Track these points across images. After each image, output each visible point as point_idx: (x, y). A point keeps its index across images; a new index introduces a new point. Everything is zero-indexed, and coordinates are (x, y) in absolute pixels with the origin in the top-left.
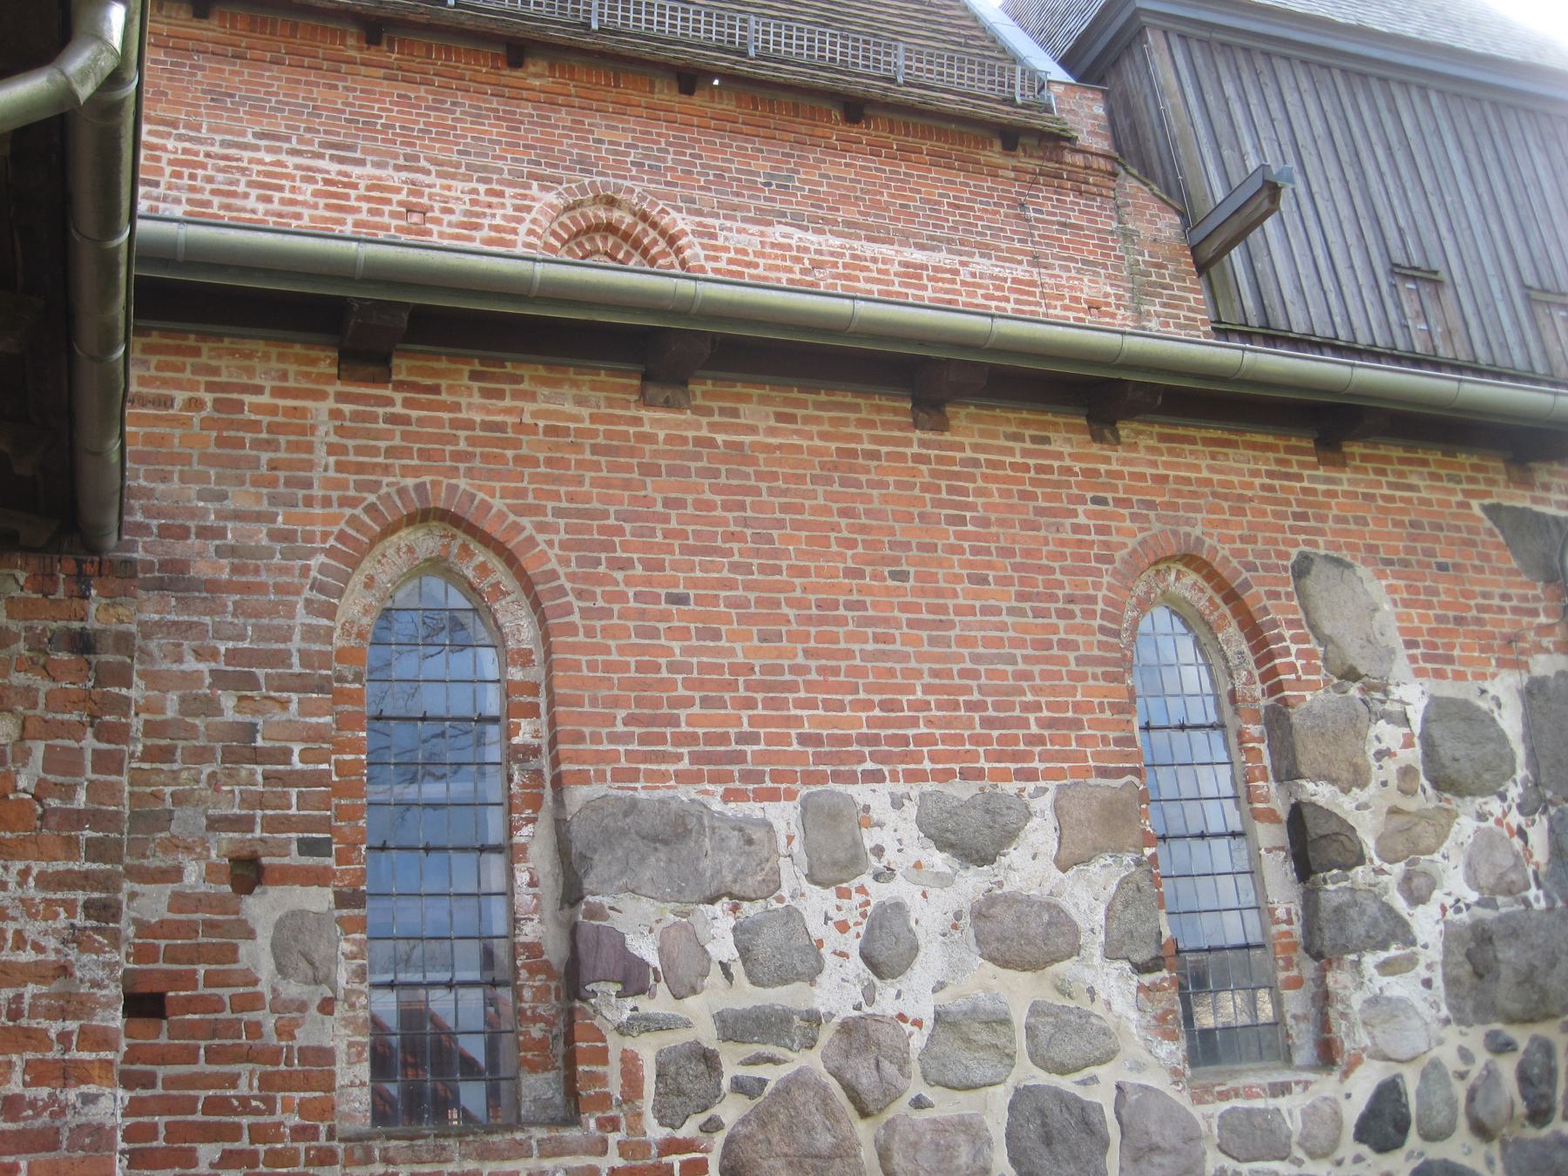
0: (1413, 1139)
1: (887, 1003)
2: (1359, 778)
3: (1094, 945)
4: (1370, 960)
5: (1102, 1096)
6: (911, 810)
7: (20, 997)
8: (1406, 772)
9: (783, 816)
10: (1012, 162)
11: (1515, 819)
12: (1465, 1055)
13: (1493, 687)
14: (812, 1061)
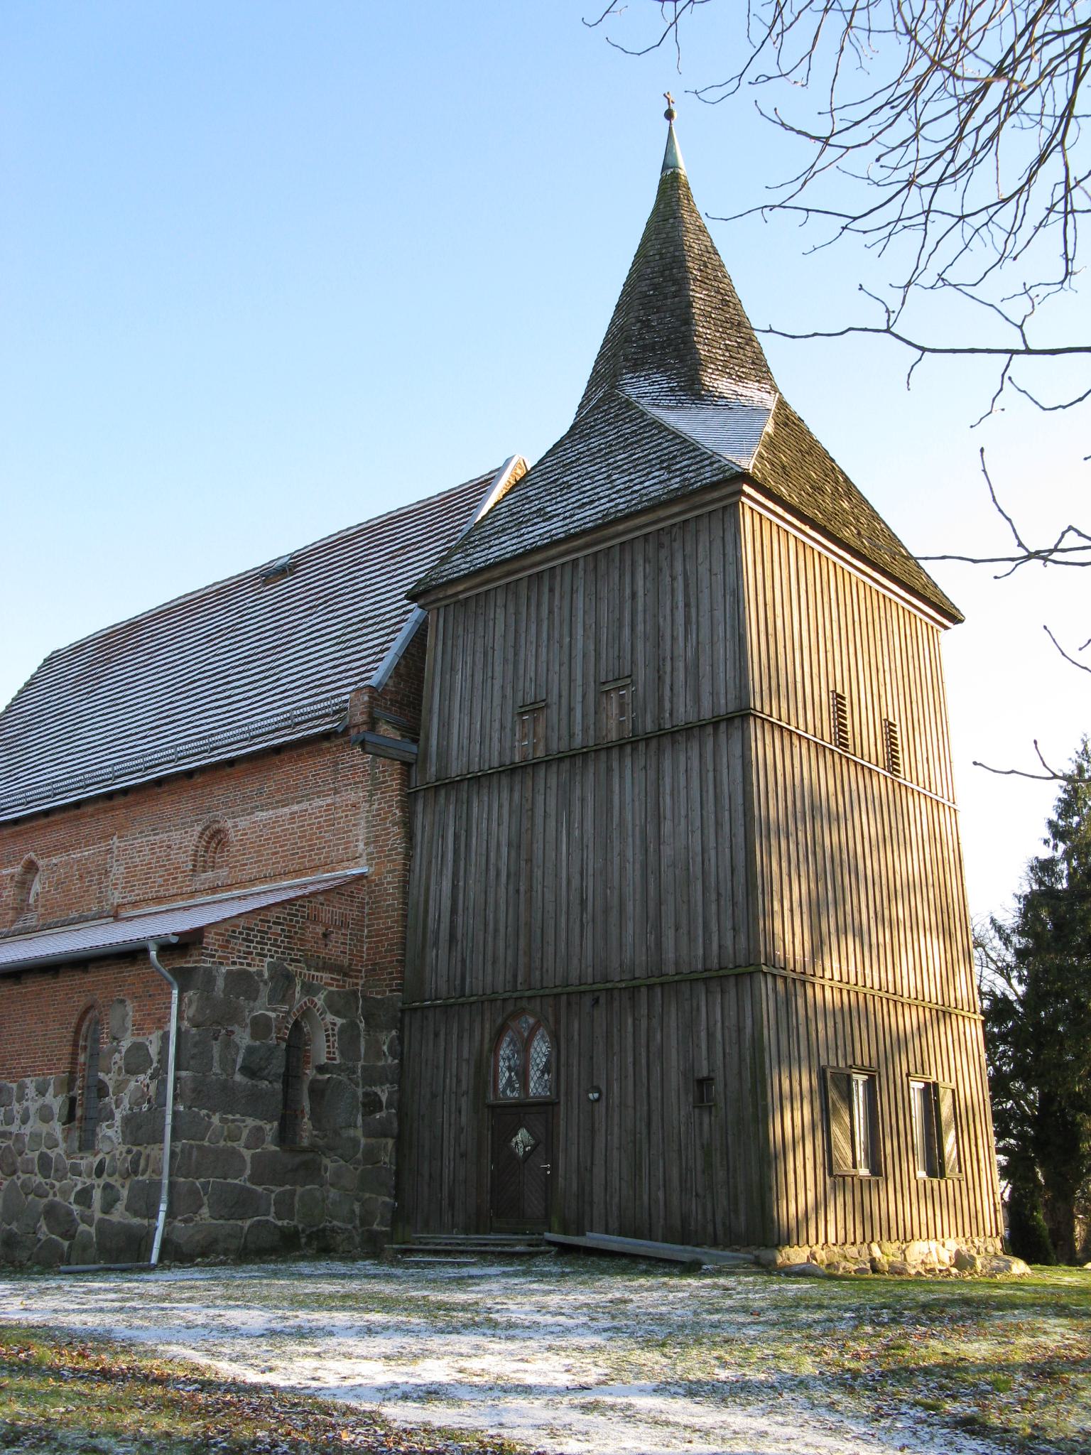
0: (105, 1175)
1: (22, 1131)
2: (108, 1072)
3: (56, 1117)
5: (53, 1155)
6: (34, 1084)
7: (293, 1193)
8: (120, 1068)
9: (14, 1085)
10: (333, 745)
11: (148, 1081)
12: (121, 1154)
13: (151, 1037)
14: (11, 1143)
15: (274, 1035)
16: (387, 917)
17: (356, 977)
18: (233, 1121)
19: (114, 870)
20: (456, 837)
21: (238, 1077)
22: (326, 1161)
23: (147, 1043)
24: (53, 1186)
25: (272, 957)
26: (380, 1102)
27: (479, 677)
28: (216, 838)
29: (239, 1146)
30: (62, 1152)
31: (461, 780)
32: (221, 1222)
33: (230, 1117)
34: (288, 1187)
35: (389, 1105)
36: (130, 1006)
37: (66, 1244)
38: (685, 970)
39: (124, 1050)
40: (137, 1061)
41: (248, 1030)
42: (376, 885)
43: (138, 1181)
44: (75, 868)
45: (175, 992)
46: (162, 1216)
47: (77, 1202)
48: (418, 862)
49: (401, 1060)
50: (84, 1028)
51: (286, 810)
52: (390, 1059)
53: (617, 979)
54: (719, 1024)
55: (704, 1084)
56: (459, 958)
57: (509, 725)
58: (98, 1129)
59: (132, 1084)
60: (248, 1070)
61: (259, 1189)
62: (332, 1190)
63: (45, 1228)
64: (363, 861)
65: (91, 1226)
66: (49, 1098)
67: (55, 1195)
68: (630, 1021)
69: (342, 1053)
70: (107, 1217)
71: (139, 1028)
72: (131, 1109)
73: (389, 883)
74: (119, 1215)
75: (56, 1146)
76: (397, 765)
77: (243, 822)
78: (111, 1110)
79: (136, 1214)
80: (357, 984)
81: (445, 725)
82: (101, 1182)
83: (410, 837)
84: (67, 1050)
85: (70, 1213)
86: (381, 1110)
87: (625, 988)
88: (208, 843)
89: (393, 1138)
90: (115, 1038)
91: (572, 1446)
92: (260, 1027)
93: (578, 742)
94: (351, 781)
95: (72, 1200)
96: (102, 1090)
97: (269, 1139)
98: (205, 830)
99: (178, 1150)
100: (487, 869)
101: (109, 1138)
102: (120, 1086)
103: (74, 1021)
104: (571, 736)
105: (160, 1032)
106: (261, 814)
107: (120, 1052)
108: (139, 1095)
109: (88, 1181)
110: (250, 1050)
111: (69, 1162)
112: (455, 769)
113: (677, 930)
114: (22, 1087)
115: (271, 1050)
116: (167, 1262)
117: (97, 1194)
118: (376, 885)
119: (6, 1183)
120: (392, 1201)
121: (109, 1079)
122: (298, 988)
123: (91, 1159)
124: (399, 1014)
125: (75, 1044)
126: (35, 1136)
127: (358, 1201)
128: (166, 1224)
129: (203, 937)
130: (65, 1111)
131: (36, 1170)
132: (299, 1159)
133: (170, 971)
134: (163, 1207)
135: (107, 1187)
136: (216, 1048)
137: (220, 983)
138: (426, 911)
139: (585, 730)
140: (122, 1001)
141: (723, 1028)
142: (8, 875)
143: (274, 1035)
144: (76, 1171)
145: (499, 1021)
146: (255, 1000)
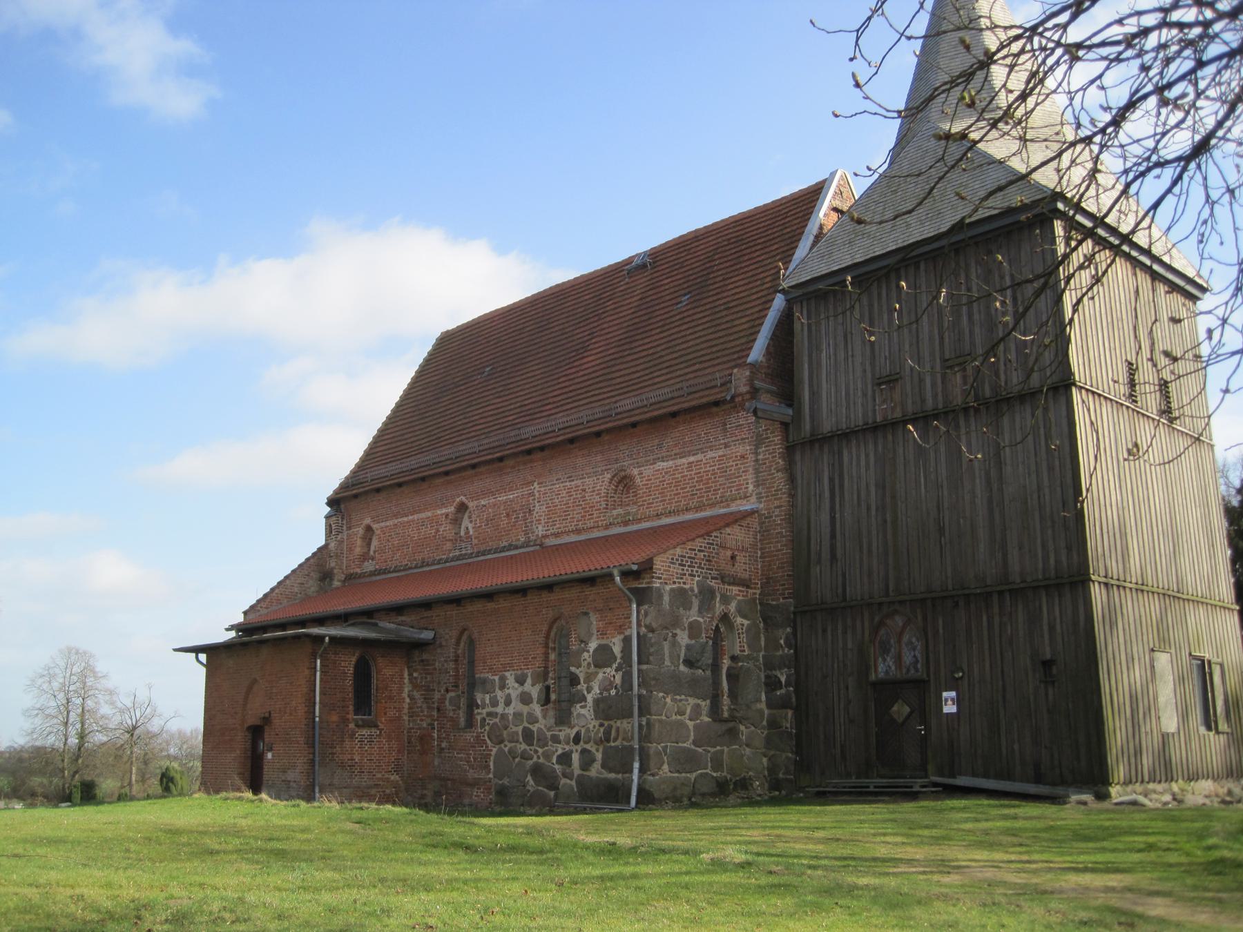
0: (582, 743)
1: (506, 711)
3: (535, 701)
4: (578, 706)
5: (535, 729)
8: (589, 664)
9: (497, 678)
11: (613, 673)
12: (594, 727)
14: (497, 720)
15: (704, 635)
16: (777, 542)
17: (755, 588)
18: (681, 700)
19: (537, 509)
20: (831, 480)
21: (682, 668)
22: (742, 728)
23: (611, 645)
24: (536, 752)
25: (699, 576)
26: (780, 682)
27: (842, 355)
28: (624, 483)
29: (685, 719)
30: (542, 727)
31: (832, 436)
32: (676, 775)
33: (678, 697)
34: (718, 748)
35: (788, 684)
36: (593, 618)
37: (552, 793)
38: (1029, 579)
39: (591, 651)
40: (603, 657)
41: (687, 632)
42: (766, 518)
43: (611, 747)
44: (502, 508)
45: (635, 606)
46: (636, 771)
47: (559, 762)
48: (800, 500)
49: (796, 652)
50: (552, 634)
51: (684, 460)
52: (786, 650)
53: (973, 586)
54: (1058, 621)
55: (1047, 664)
56: (840, 573)
57: (870, 393)
58: (572, 709)
59: (600, 676)
60: (689, 663)
61: (700, 750)
62: (748, 750)
63: (532, 782)
64: (753, 499)
65: (571, 780)
66: (528, 686)
67: (538, 757)
68: (985, 618)
69: (749, 646)
70: (585, 773)
71: (603, 634)
72: (601, 693)
73: (776, 516)
74: (595, 771)
75: (537, 722)
76: (777, 425)
77: (648, 471)
78: (584, 695)
79: (610, 770)
80: (755, 594)
81: (815, 395)
82: (579, 748)
83: (792, 479)
84: (540, 651)
85: (554, 771)
86: (781, 688)
87: (979, 594)
88: (617, 486)
89: (791, 708)
90: (582, 641)
91: (515, 922)
92: (694, 629)
93: (930, 404)
94: (739, 437)
95: (554, 760)
96: (574, 680)
97: (704, 712)
98: (613, 477)
99: (644, 723)
100: (859, 504)
101: (584, 715)
102: (589, 678)
103: (545, 628)
104: (923, 401)
105: (622, 637)
106: (662, 464)
107: (588, 651)
108: (608, 683)
109: (567, 748)
110: (688, 647)
111: (549, 734)
112: (827, 426)
113: (1020, 549)
114: (503, 679)
115: (704, 646)
116: (641, 806)
117: (575, 757)
118: (766, 518)
119: (495, 750)
120: (794, 756)
121: (580, 673)
122: (718, 599)
123: (568, 731)
124: (792, 616)
125: (546, 646)
126: (518, 715)
127: (765, 756)
128: (640, 778)
129: (653, 564)
130: (543, 697)
131: (521, 739)
132: (725, 727)
133: (628, 589)
134: (636, 765)
135: (584, 751)
136: (666, 645)
137: (666, 598)
138: (809, 539)
139: (935, 396)
140: (586, 614)
141: (1061, 622)
142: (442, 515)
143: (704, 635)
144: (556, 740)
145: (877, 619)
146: (690, 609)
